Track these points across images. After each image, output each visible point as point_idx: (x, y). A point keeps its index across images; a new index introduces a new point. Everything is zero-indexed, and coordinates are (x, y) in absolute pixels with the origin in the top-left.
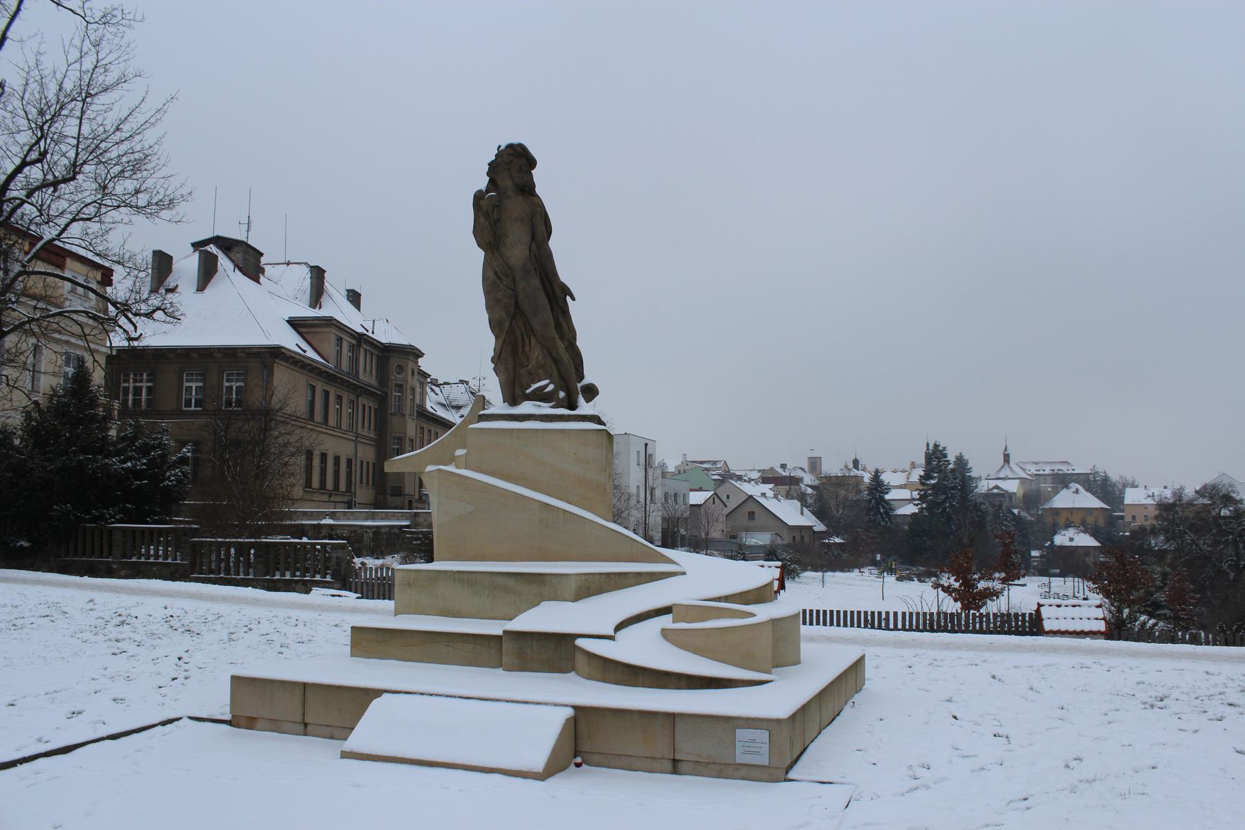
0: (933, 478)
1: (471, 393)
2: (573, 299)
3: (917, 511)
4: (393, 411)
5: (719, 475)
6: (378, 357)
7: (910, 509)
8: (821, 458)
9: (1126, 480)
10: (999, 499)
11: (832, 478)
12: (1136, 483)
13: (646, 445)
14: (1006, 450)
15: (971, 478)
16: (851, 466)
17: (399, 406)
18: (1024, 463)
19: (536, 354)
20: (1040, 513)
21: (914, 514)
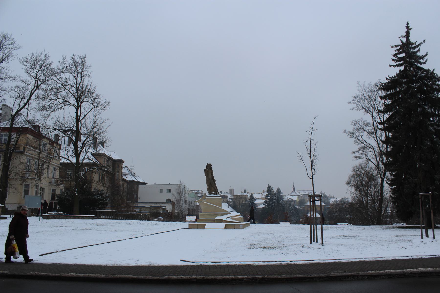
0: (269, 196)
1: (129, 170)
3: (264, 207)
4: (116, 179)
5: (200, 195)
6: (112, 163)
7: (262, 206)
8: (233, 189)
9: (331, 196)
10: (290, 202)
11: (238, 196)
12: (334, 197)
13: (184, 187)
14: (293, 186)
15: (282, 196)
16: (243, 192)
17: (118, 177)
18: (300, 190)
19: (213, 189)
20: (304, 207)
21: (263, 207)
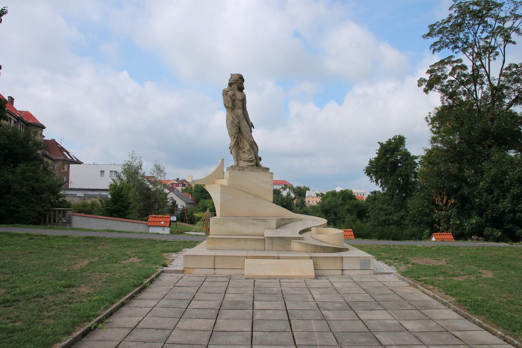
2: (254, 128)
